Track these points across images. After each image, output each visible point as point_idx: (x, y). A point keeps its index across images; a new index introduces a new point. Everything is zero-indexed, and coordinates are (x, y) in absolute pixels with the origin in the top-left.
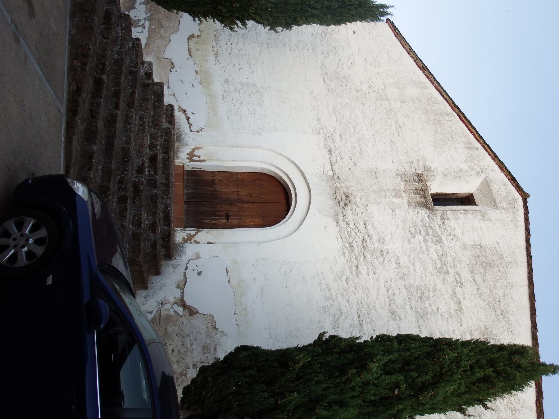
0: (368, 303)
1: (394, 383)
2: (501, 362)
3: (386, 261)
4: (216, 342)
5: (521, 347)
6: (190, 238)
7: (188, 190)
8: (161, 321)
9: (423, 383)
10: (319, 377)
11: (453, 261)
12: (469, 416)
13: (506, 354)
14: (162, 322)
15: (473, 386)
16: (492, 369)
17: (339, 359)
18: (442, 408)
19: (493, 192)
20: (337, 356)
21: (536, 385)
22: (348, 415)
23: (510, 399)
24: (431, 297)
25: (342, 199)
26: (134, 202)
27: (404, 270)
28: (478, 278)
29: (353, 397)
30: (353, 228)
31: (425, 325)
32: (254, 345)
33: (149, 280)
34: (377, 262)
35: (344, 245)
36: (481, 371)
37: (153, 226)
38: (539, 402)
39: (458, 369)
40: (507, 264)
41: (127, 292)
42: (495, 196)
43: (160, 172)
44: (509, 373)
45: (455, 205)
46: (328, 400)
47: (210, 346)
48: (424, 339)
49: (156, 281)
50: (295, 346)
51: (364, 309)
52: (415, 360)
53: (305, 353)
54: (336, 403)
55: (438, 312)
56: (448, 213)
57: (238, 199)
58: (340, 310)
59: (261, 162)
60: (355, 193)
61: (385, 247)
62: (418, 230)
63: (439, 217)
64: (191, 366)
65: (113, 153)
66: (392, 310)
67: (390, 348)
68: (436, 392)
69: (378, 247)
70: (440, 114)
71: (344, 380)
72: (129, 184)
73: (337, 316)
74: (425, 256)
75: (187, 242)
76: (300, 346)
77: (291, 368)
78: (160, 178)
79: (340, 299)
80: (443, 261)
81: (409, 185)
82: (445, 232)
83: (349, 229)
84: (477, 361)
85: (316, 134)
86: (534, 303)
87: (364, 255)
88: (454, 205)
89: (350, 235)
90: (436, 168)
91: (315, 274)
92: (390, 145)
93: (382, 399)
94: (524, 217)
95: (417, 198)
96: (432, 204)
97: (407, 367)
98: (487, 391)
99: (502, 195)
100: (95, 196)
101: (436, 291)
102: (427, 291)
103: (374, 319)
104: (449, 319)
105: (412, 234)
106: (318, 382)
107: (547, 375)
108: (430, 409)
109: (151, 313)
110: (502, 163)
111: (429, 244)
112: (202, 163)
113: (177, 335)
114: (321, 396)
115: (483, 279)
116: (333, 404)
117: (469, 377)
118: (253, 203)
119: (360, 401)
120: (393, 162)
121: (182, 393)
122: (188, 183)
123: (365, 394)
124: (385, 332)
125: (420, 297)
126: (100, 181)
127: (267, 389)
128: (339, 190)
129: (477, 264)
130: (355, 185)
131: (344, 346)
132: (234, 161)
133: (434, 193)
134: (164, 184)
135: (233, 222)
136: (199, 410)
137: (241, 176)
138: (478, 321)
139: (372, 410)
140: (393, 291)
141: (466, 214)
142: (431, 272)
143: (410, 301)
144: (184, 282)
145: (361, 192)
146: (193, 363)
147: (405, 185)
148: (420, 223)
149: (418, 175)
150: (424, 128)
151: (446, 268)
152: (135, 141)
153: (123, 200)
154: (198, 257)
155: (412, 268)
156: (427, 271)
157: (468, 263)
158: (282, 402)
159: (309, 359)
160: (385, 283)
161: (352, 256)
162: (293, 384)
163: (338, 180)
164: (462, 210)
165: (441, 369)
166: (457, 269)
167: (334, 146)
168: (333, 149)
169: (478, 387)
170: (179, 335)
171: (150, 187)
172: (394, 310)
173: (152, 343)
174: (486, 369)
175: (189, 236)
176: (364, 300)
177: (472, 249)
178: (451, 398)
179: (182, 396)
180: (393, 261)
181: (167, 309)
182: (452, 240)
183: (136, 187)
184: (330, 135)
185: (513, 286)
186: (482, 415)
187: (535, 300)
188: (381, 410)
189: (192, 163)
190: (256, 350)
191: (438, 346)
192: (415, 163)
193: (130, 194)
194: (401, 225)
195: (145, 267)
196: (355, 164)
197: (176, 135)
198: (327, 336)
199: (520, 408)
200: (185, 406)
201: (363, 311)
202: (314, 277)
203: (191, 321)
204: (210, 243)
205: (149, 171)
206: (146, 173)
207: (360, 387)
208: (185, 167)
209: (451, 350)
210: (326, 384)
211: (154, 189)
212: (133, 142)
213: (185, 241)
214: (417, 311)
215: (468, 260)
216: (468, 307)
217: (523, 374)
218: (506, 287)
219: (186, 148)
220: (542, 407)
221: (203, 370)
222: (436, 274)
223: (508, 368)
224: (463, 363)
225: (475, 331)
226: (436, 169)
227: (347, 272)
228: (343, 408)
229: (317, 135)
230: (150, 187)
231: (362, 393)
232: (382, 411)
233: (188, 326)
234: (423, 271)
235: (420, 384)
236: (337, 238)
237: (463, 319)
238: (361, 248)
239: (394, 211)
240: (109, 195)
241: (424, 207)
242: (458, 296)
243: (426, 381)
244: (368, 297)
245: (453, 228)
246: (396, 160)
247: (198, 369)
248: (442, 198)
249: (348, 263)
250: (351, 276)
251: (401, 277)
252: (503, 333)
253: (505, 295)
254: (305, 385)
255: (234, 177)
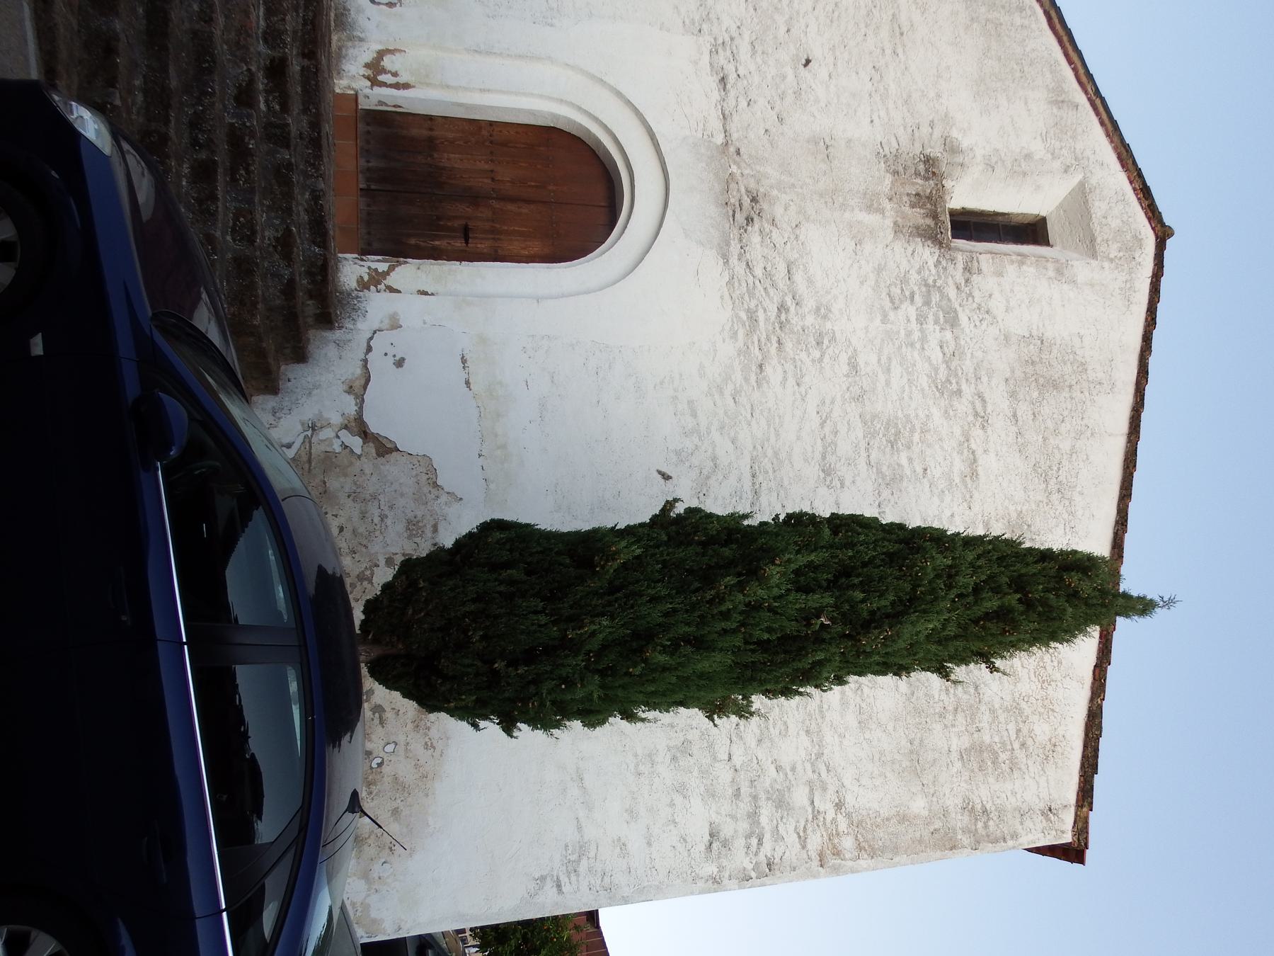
0: (778, 446)
1: (813, 611)
2: (1039, 584)
3: (827, 357)
4: (437, 515)
5: (1086, 558)
6: (376, 279)
7: (368, 162)
8: (313, 464)
9: (872, 613)
10: (659, 589)
11: (976, 369)
12: (955, 682)
13: (1052, 568)
14: (315, 468)
15: (973, 625)
16: (1018, 596)
17: (704, 555)
18: (904, 664)
19: (1094, 216)
20: (699, 549)
21: (1100, 637)
22: (710, 666)
23: (1042, 659)
24: (914, 444)
25: (741, 205)
26: (234, 180)
27: (864, 381)
28: (1024, 410)
29: (725, 631)
30: (760, 276)
31: (892, 503)
32: (519, 521)
33: (281, 374)
34: (808, 360)
35: (737, 316)
36: (996, 598)
37: (285, 244)
38: (1101, 670)
39: (950, 590)
40: (1092, 386)
41: (236, 395)
42: (1096, 227)
43: (296, 107)
44: (1051, 607)
45: (1000, 240)
46: (672, 636)
47: (425, 521)
48: (887, 528)
49: (297, 376)
50: (610, 526)
51: (767, 459)
52: (862, 567)
53: (630, 541)
54: (688, 642)
55: (924, 477)
56: (982, 257)
57: (493, 189)
58: (714, 459)
59: (550, 98)
60: (775, 192)
61: (829, 325)
62: (907, 293)
63: (960, 266)
64: (382, 562)
65: (170, 46)
66: (828, 465)
67: (814, 539)
68: (897, 632)
69: (812, 325)
70: (1003, 7)
71: (708, 597)
72: (218, 132)
73: (705, 472)
74: (916, 354)
75: (368, 289)
76: (621, 526)
77: (598, 569)
78: (296, 123)
79: (715, 435)
80: (953, 368)
81: (902, 184)
82: (967, 301)
83: (750, 280)
84: (991, 577)
85: (693, 34)
86: (1132, 473)
87: (779, 341)
88: (999, 240)
89: (751, 293)
90: (970, 147)
91: (665, 377)
92: (871, 79)
93: (785, 639)
94: (1151, 283)
95: (917, 217)
96: (949, 233)
97: (844, 580)
98: (999, 637)
99: (1113, 225)
100: (135, 156)
101: (929, 431)
102: (908, 430)
103: (786, 483)
104: (947, 492)
105: (892, 301)
106: (654, 600)
107: (1127, 616)
108: (878, 664)
109: (289, 446)
110: (1127, 148)
111: (929, 326)
112: (402, 93)
113: (349, 497)
114: (657, 627)
115: (1034, 414)
116: (682, 644)
117: (968, 607)
118: (528, 201)
119: (738, 641)
120: (872, 121)
121: (364, 612)
122: (368, 142)
123: (750, 627)
124: (807, 509)
125: (890, 442)
126: (141, 120)
127: (545, 609)
128: (737, 183)
129: (1026, 378)
130: (775, 174)
131: (716, 530)
132: (484, 90)
133: (958, 207)
134: (307, 140)
135: (479, 246)
136: (400, 646)
137: (501, 131)
138: (1007, 501)
139: (761, 659)
140: (835, 424)
141: (1022, 263)
142: (923, 390)
143: (867, 450)
144: (363, 382)
145: (788, 190)
146: (386, 557)
147: (892, 182)
148: (914, 277)
149: (929, 161)
150: (958, 40)
151: (957, 383)
152: (226, 17)
153: (204, 173)
154: (395, 325)
155: (882, 378)
156: (914, 388)
157: (1008, 375)
158: (577, 634)
159: (638, 552)
160: (818, 406)
161: (753, 343)
162: (600, 602)
163: (737, 158)
164: (1014, 253)
165: (914, 589)
166: (980, 387)
167: (734, 70)
168: (732, 78)
169: (983, 627)
170: (353, 496)
171: (273, 144)
172: (832, 467)
173: (289, 497)
174: (1005, 594)
175: (373, 274)
176: (768, 440)
177: (1022, 345)
178: (924, 646)
179: (363, 617)
180: (844, 358)
181: (325, 440)
182: (981, 321)
183: (236, 140)
184: (727, 39)
185: (1095, 435)
186: (982, 686)
187: (1135, 466)
188: (779, 661)
189: (377, 90)
190: (525, 529)
191: (915, 543)
192: (925, 130)
193: (222, 157)
194: (872, 277)
195: (271, 341)
196: (780, 119)
197: (333, 10)
198: (680, 509)
199: (1059, 678)
200: (370, 637)
201: (763, 464)
202: (662, 383)
203: (382, 467)
204: (425, 293)
205: (266, 101)
206: (259, 107)
207: (741, 613)
208: (361, 99)
209: (941, 552)
210: (671, 603)
211: (282, 150)
212: (221, 20)
213: (364, 285)
214: (879, 472)
215: (1009, 370)
216: (990, 471)
217: (1081, 610)
218: (1079, 435)
219: (360, 49)
220: (1105, 680)
221: (409, 567)
222: (934, 395)
223: (1052, 596)
224: (961, 580)
225: (997, 521)
226: (971, 149)
227: (738, 377)
228: (702, 651)
229: (695, 37)
230: (271, 145)
231: (743, 624)
232: (780, 663)
233: (374, 479)
234: (907, 386)
235: (865, 614)
236: (722, 297)
237: (976, 495)
238: (773, 324)
239: (860, 244)
240: (168, 157)
241: (929, 239)
242: (973, 446)
243: (878, 609)
244: (777, 435)
245: (989, 293)
246: (879, 118)
247: (397, 568)
248: (975, 223)
249: (742, 357)
250: (745, 388)
251: (856, 397)
252: (1053, 530)
253: (1073, 451)
254: (625, 604)
255: (484, 133)
